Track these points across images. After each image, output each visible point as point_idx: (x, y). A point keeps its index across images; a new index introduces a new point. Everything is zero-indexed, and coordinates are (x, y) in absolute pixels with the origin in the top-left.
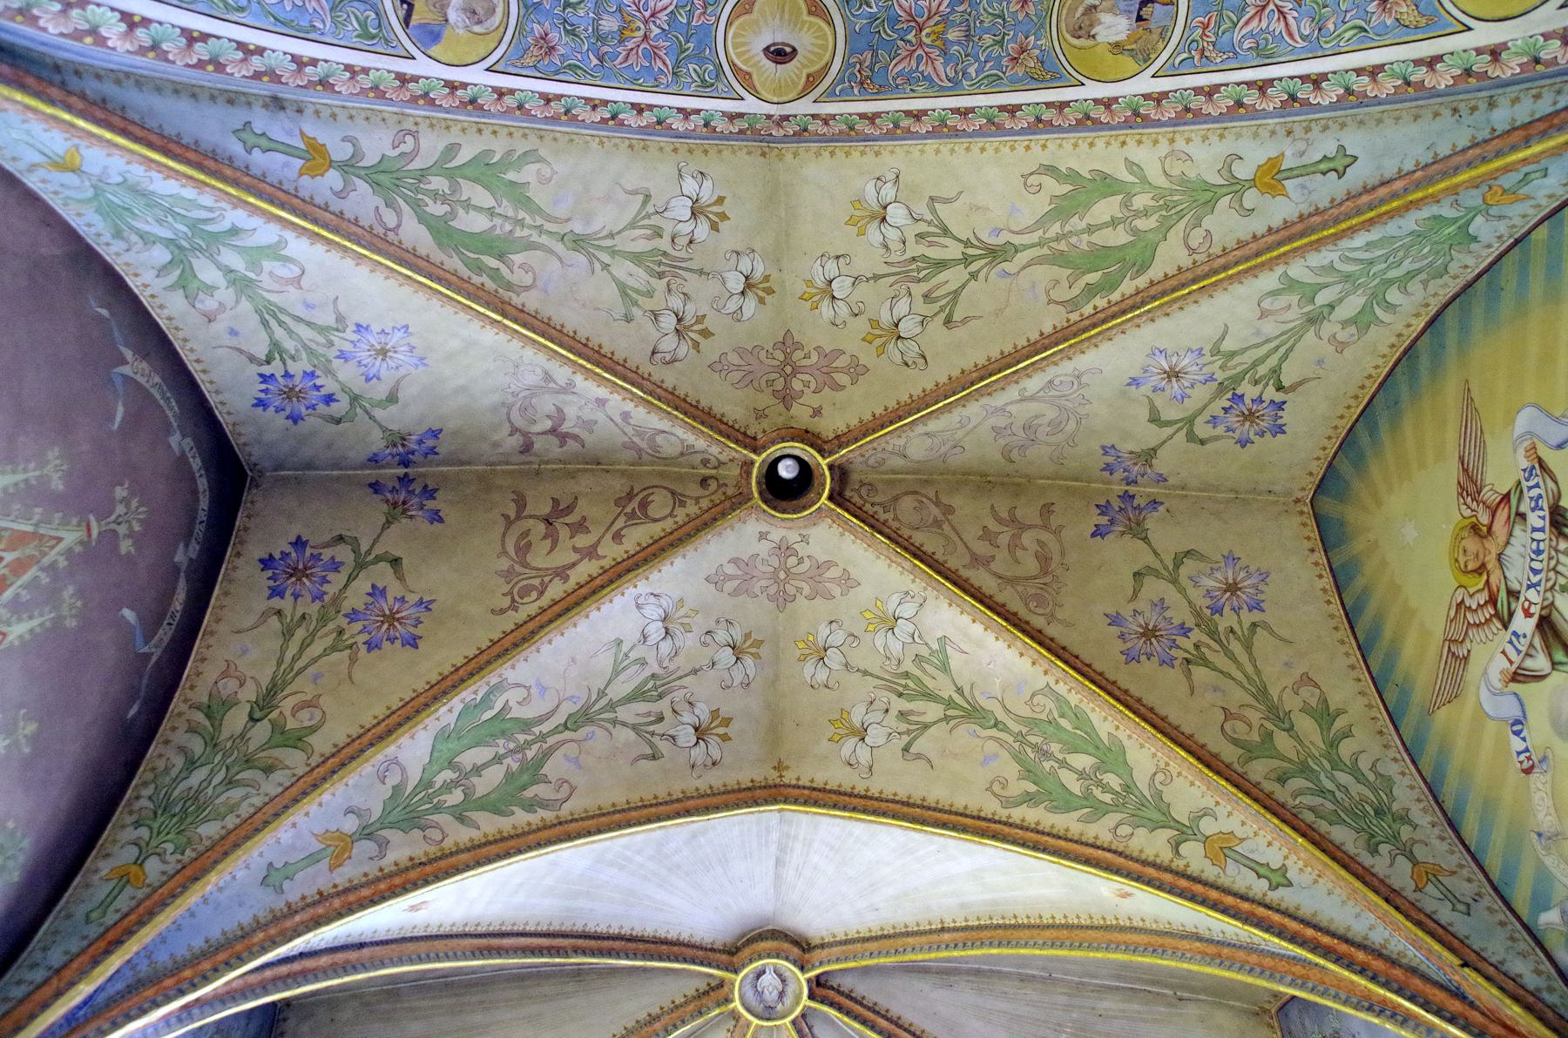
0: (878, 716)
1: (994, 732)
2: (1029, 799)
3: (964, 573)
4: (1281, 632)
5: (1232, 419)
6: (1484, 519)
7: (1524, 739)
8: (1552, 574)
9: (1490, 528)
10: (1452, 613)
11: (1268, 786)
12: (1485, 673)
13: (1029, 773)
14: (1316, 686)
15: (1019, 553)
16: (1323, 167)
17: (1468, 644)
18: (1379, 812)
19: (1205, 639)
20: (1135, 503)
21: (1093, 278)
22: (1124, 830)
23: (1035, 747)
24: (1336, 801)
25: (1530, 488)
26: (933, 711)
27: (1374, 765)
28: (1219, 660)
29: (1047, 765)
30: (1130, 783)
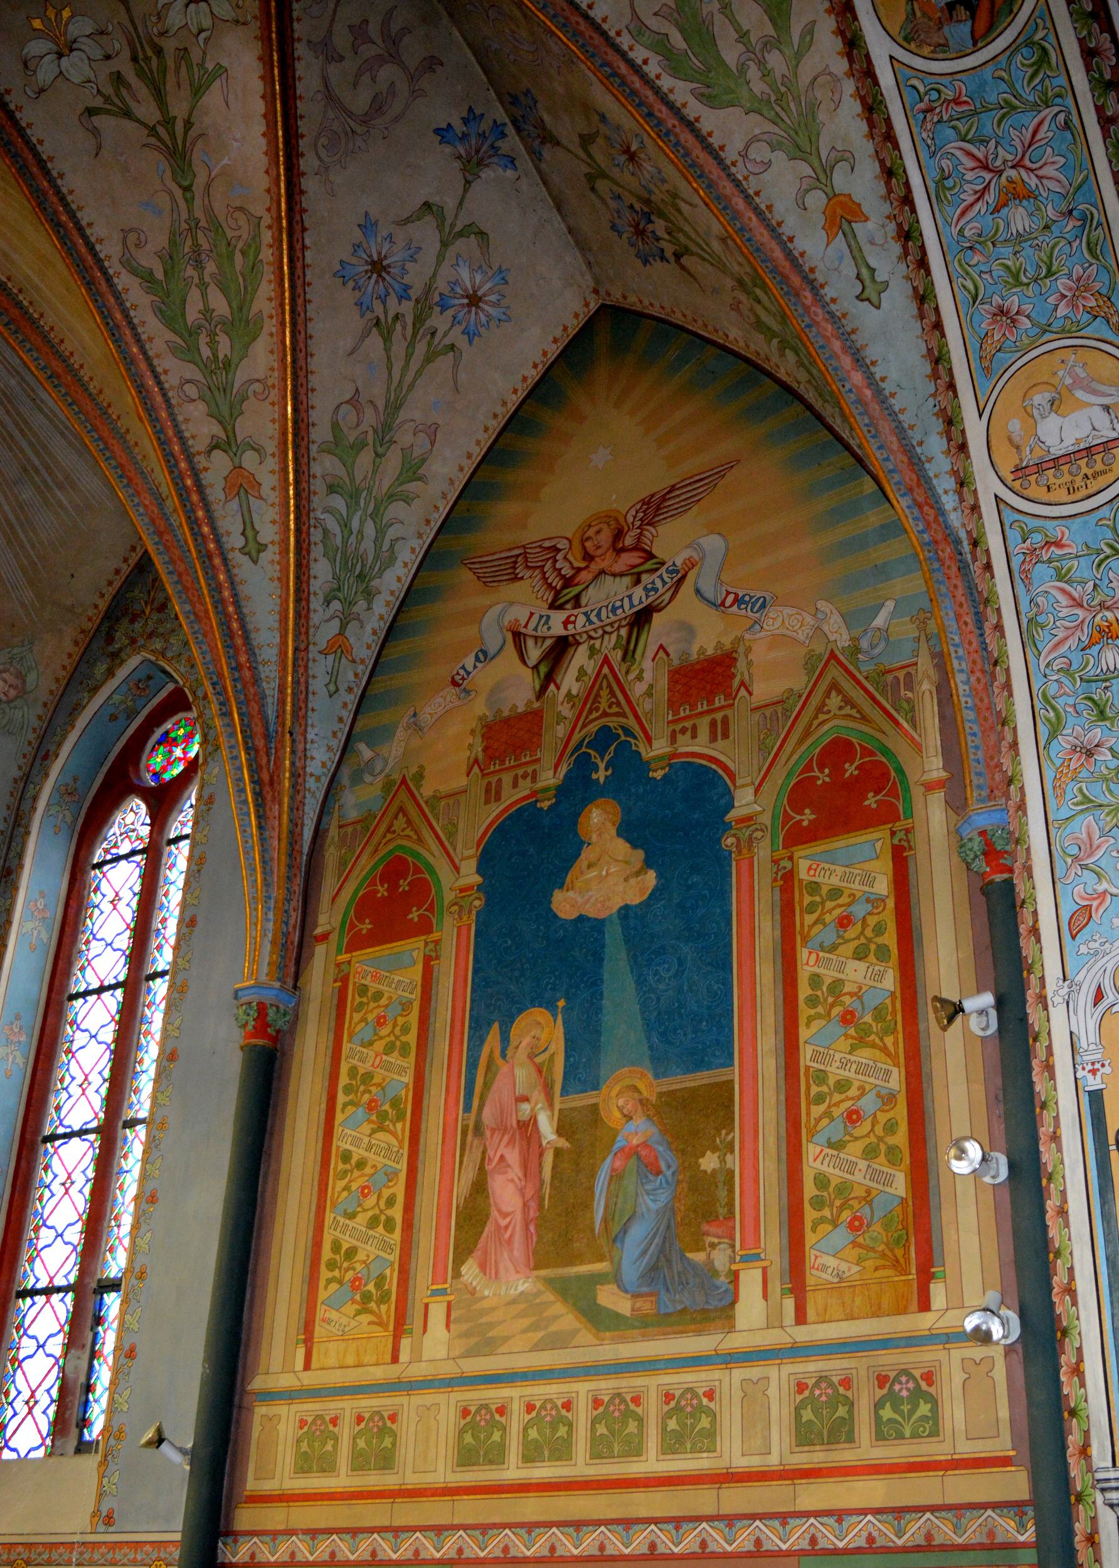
0: (98, 54)
1: (178, 193)
2: (147, 278)
3: (300, 49)
4: (462, 377)
5: (628, 215)
6: (629, 541)
7: (475, 667)
8: (600, 632)
9: (624, 550)
10: (547, 544)
11: (318, 485)
12: (512, 603)
13: (170, 259)
14: (433, 443)
15: (366, 79)
16: (865, 272)
17: (528, 574)
18: (361, 577)
19: (409, 320)
20: (499, 144)
21: (677, 40)
22: (191, 391)
23: (196, 245)
24: (345, 542)
25: (661, 577)
26: (147, 110)
27: (397, 539)
28: (399, 347)
29: (190, 272)
30: (235, 361)
